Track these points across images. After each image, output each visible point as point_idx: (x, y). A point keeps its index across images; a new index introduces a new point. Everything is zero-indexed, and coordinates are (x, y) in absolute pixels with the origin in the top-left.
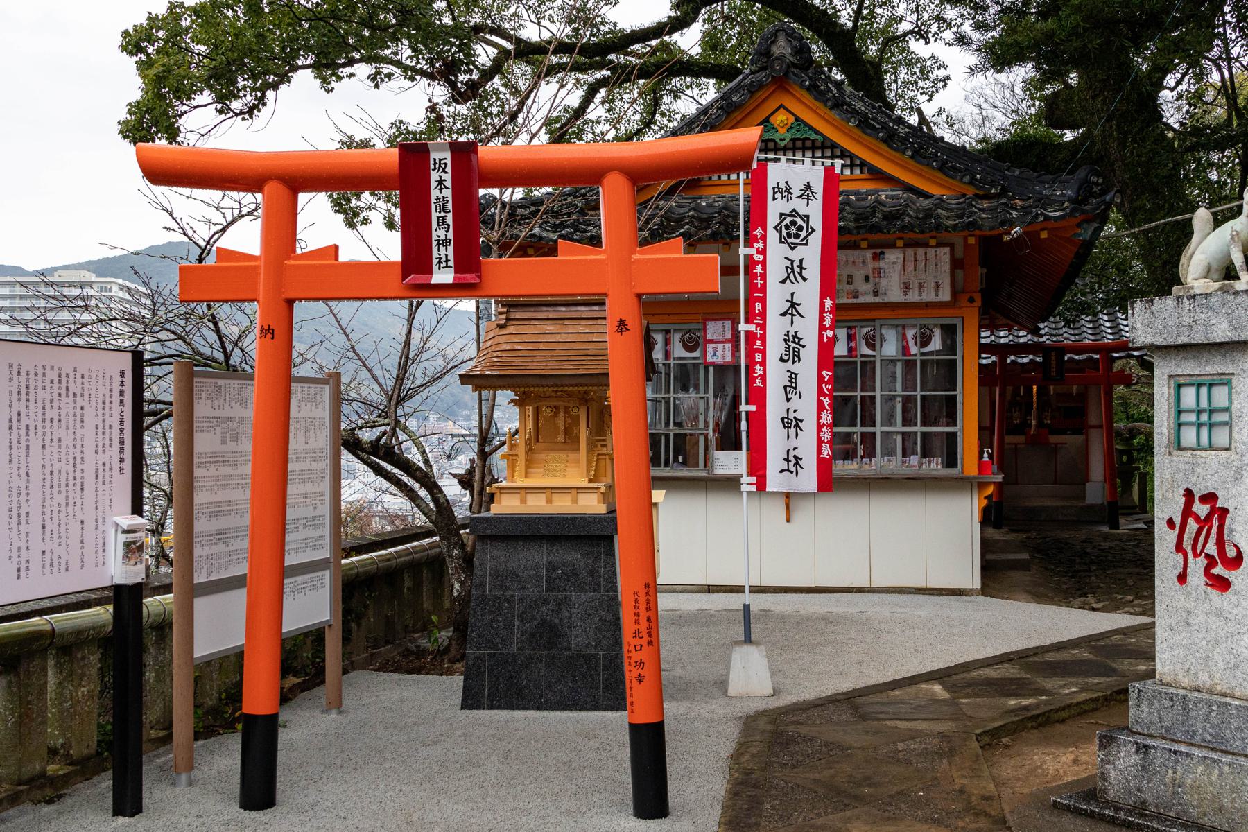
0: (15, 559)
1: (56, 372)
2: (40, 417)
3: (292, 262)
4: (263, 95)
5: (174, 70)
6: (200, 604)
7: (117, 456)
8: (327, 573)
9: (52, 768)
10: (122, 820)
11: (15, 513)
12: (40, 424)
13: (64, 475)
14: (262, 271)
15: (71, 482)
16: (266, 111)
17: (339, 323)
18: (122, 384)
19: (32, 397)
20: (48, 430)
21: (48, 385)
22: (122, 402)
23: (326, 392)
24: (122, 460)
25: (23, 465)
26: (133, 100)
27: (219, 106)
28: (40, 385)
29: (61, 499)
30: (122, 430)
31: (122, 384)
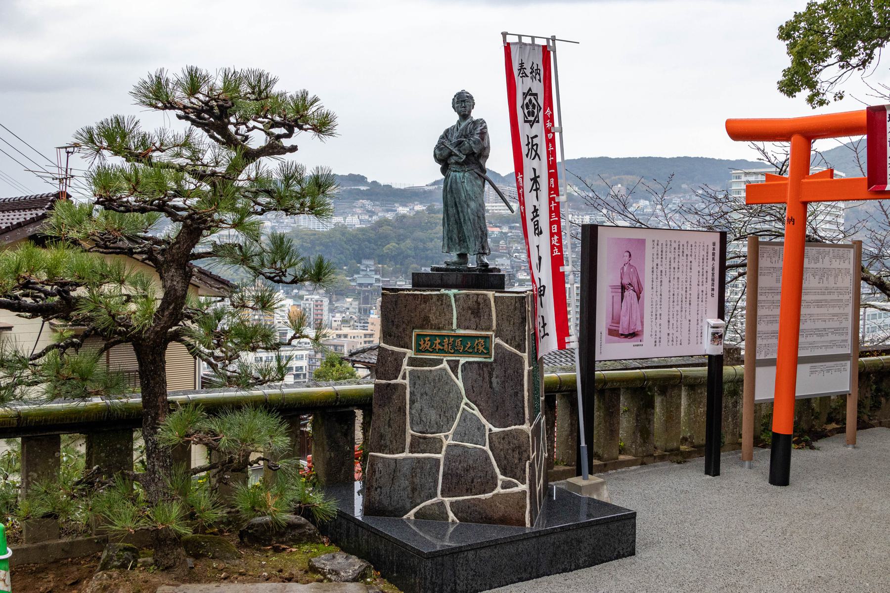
0: (654, 336)
1: (677, 244)
2: (668, 267)
3: (806, 180)
4: (872, 52)
5: (807, 49)
6: (759, 371)
7: (710, 287)
8: (849, 363)
9: (683, 448)
10: (708, 477)
11: (654, 314)
12: (668, 270)
13: (680, 297)
14: (789, 187)
15: (684, 300)
16: (874, 62)
17: (882, 207)
18: (714, 249)
19: (664, 257)
20: (672, 273)
21: (673, 250)
22: (713, 259)
23: (851, 253)
24: (713, 290)
25: (659, 290)
26: (786, 68)
27: (842, 64)
28: (668, 250)
29: (679, 308)
30: (713, 274)
31: (714, 249)
